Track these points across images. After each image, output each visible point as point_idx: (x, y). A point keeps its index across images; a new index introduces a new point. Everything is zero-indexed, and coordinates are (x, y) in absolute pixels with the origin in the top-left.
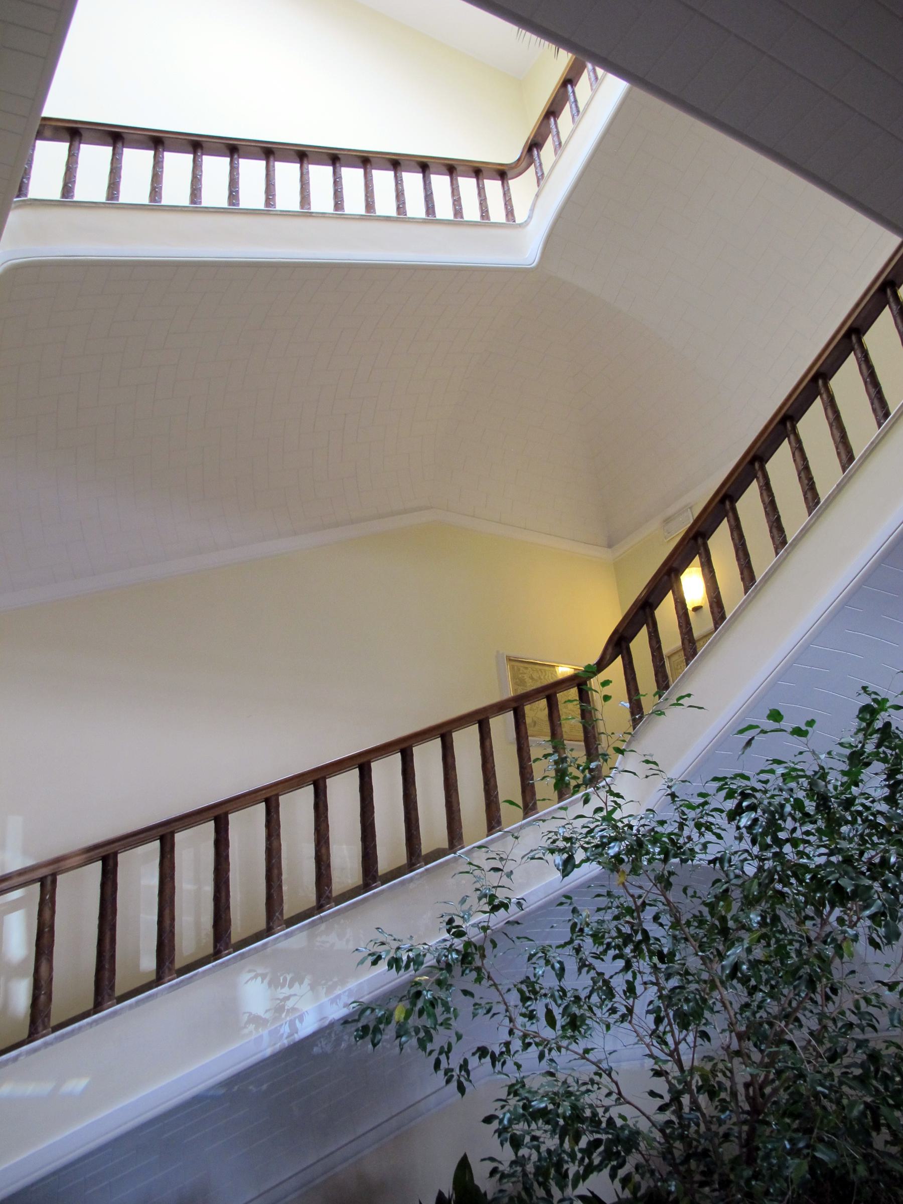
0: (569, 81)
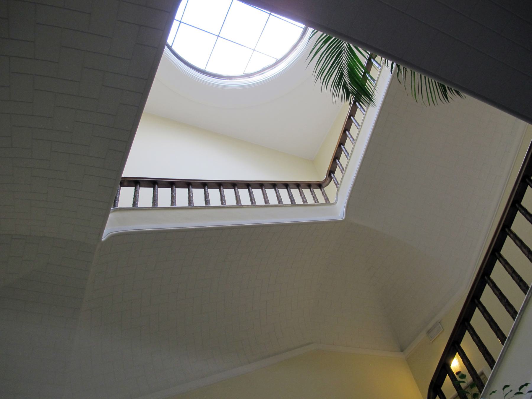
0: (352, 114)
